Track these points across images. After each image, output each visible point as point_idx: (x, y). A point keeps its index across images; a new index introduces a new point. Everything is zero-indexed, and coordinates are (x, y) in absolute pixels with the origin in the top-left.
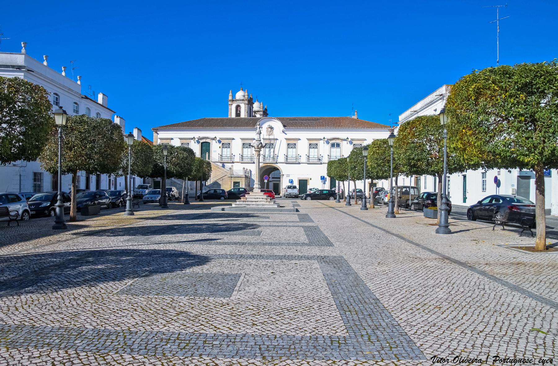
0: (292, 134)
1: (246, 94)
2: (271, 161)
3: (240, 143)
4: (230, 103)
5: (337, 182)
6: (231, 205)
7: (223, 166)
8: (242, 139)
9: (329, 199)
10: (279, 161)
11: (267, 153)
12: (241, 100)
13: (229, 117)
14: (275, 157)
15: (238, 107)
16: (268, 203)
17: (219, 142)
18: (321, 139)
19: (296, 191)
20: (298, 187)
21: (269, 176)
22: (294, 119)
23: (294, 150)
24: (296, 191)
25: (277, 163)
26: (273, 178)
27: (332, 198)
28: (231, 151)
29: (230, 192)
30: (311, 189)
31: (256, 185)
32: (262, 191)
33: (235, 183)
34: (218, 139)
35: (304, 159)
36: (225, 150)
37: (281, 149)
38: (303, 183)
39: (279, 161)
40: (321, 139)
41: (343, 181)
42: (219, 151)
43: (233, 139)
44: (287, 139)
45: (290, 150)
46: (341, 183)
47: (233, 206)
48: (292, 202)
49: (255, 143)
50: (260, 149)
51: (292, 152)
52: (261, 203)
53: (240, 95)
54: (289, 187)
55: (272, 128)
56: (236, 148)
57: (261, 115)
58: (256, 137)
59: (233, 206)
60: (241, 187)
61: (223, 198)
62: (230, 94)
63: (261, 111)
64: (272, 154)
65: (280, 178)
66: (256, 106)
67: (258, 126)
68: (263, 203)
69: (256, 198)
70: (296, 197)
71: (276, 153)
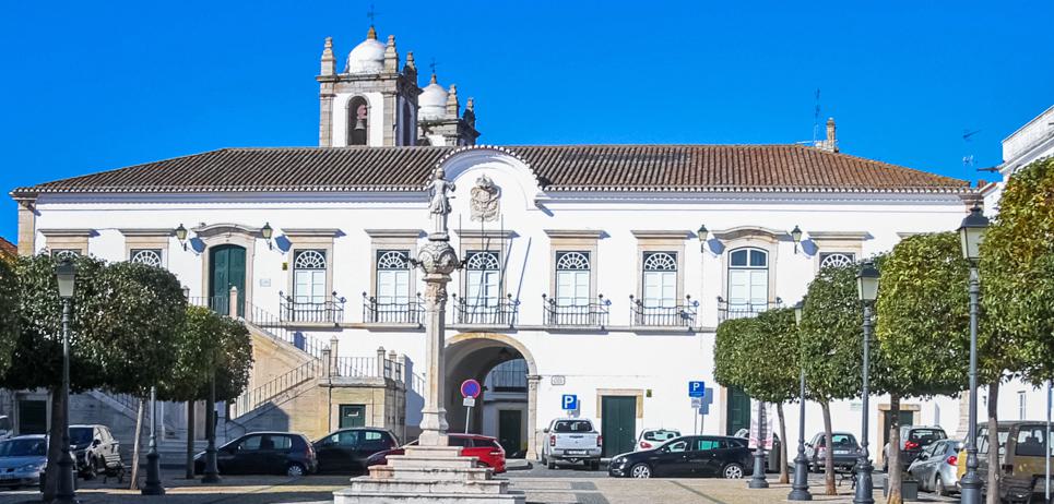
0: (575, 215)
1: (391, 53)
2: (490, 320)
4: (325, 89)
5: (755, 404)
7: (299, 343)
9: (721, 475)
11: (474, 291)
12: (369, 78)
13: (323, 144)
14: (507, 306)
16: (477, 490)
17: (284, 244)
18: (691, 235)
19: (589, 443)
20: (597, 425)
21: (480, 380)
22: (584, 155)
24: (589, 443)
25: (512, 329)
26: (497, 389)
27: (734, 470)
28: (329, 282)
29: (325, 447)
30: (649, 435)
31: (431, 418)
32: (452, 442)
33: (346, 409)
34: (277, 233)
35: (620, 314)
36: (305, 277)
37: (529, 276)
38: (619, 410)
39: (522, 320)
40: (691, 235)
41: (779, 401)
42: (282, 281)
43: (339, 234)
44: (553, 234)
45: (567, 278)
46: (771, 409)
48: (575, 486)
49: (424, 250)
50: (446, 272)
51: (573, 286)
52: (451, 489)
53: (364, 56)
54: (563, 427)
55: (492, 189)
56: (351, 268)
57: (448, 137)
58: (431, 225)
61: (296, 470)
62: (327, 53)
63: (448, 122)
64: (494, 292)
65: (524, 390)
66: (430, 102)
67: (439, 183)
68: (460, 489)
70: (591, 465)
71: (511, 288)
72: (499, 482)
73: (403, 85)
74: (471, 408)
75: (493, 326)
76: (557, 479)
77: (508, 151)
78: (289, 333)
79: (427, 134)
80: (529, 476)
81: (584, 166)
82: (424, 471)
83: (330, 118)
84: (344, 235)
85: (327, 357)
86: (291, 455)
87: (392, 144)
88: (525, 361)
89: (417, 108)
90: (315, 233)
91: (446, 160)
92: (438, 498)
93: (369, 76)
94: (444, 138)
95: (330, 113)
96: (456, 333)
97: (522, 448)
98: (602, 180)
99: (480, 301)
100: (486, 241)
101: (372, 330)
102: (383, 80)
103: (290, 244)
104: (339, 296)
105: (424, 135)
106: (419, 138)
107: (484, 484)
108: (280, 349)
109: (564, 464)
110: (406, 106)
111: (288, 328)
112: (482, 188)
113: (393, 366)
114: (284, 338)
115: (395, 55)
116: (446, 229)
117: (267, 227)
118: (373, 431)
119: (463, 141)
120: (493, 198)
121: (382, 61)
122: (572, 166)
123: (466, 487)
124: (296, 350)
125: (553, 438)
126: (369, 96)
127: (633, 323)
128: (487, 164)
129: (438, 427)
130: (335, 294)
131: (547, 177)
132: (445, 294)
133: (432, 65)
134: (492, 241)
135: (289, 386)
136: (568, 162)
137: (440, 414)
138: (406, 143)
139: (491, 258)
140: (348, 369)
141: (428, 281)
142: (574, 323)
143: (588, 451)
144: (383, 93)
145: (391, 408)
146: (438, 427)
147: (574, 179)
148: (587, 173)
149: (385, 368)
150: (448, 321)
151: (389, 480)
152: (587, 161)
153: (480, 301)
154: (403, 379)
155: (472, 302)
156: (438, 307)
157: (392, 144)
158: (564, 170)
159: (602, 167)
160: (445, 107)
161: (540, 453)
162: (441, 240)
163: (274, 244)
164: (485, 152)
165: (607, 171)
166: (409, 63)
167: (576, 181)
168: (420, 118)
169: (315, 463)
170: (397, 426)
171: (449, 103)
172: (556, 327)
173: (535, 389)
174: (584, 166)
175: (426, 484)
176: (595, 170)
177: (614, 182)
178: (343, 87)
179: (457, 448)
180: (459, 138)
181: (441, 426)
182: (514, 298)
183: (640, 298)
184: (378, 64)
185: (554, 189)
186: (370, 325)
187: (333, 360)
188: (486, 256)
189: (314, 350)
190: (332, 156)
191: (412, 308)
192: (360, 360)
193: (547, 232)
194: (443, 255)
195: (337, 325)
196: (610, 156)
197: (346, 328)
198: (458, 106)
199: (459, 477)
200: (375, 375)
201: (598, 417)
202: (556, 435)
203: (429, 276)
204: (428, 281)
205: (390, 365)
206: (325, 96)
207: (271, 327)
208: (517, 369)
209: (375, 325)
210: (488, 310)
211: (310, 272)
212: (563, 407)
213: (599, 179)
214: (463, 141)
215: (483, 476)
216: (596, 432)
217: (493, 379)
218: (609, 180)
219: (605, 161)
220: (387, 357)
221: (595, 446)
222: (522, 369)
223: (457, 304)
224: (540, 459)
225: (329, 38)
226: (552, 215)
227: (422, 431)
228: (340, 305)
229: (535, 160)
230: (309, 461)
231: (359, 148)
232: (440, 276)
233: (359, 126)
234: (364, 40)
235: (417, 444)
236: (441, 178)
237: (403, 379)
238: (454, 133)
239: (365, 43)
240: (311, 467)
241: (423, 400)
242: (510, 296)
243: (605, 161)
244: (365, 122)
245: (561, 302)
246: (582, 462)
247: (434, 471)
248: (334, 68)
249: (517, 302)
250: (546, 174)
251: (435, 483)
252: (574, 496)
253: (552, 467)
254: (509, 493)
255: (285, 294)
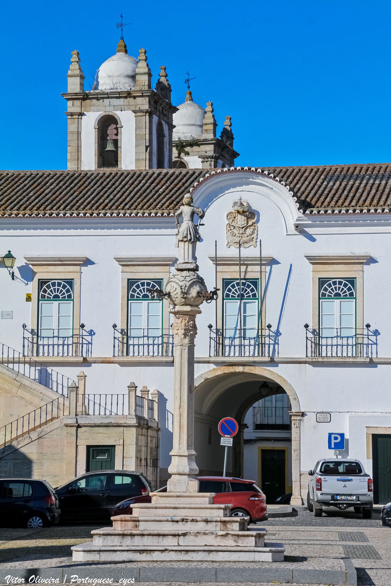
1: (142, 67)
2: (250, 353)
3: (119, 278)
4: (73, 107)
6: (66, 551)
7: (45, 380)
8: (125, 263)
10: (283, 353)
11: (231, 322)
13: (71, 167)
14: (267, 338)
15: (107, 124)
16: (230, 542)
17: (27, 273)
19: (359, 487)
20: (368, 467)
21: (240, 417)
23: (349, 305)
24: (359, 487)
25: (272, 362)
26: (259, 427)
28: (76, 314)
29: (69, 493)
31: (180, 461)
32: (204, 487)
33: (93, 451)
34: (20, 262)
36: (51, 308)
37: (291, 305)
39: (283, 353)
43: (87, 262)
44: (315, 261)
47: (78, 557)
48: (343, 537)
49: (175, 283)
50: (195, 304)
52: (201, 541)
53: (113, 72)
54: (329, 469)
55: (250, 214)
56: (101, 298)
57: (205, 158)
58: (181, 253)
59: (78, 557)
60: (118, 467)
62: (74, 68)
63: (205, 142)
64: (252, 323)
65: (287, 427)
66: (185, 122)
67: (186, 210)
68: (211, 540)
69: (182, 516)
70: (362, 512)
71: (271, 318)
72: (254, 533)
73: (156, 102)
74: (229, 447)
75: (251, 359)
76: (323, 528)
77: (266, 172)
78: (33, 369)
79: (182, 155)
80: (294, 524)
81: (348, 188)
82: (173, 521)
83: (79, 139)
84: (93, 263)
85: (73, 395)
86: (30, 504)
87: (144, 167)
88: (288, 396)
89: (172, 127)
90: (62, 262)
91: (200, 184)
92: (187, 551)
93: (119, 93)
94: (201, 160)
95: (79, 133)
96: (212, 366)
97: (287, 493)
98: (368, 202)
99: (238, 332)
100: (243, 268)
101: (123, 364)
102: (135, 97)
103: (34, 273)
104: (87, 328)
105: (179, 157)
106: (174, 159)
107: (238, 536)
108: (22, 386)
109: (334, 510)
110: (160, 125)
111: (31, 364)
112: (238, 212)
113: (146, 403)
114: (27, 374)
115: (146, 70)
116: (195, 258)
117: (9, 256)
118: (123, 474)
119: (220, 162)
120: (250, 223)
121: (133, 77)
122: (335, 187)
123: (219, 539)
124: (41, 388)
125: (319, 481)
126: (120, 115)
127: (212, 354)
128: (244, 187)
129: (187, 471)
130: (82, 326)
131: (308, 199)
132: (195, 327)
133: (187, 81)
134: (250, 268)
135: (32, 426)
136: (331, 184)
137: (189, 457)
138: (160, 165)
139: (249, 286)
140: (97, 406)
141: (175, 313)
142: (350, 354)
143: (358, 496)
144: (135, 112)
145: (143, 449)
146: (187, 471)
147: (337, 202)
148: (351, 194)
149: (136, 405)
150: (200, 353)
151: (134, 532)
152: (351, 182)
153: (238, 332)
154: (156, 417)
155: (229, 333)
156: (187, 341)
157: (144, 167)
158: (326, 192)
159: (368, 187)
160: (201, 126)
161: (305, 498)
162: (189, 270)
163: (17, 274)
164: (247, 175)
165: (374, 191)
166: (163, 79)
167: (340, 202)
168: (175, 137)
169: (57, 512)
170: (150, 469)
171: (205, 121)
172: (320, 360)
173: (299, 427)
174: (348, 188)
175: (174, 535)
176: (360, 190)
177: (381, 203)
178: (91, 106)
179: (208, 494)
180: (216, 159)
181: (191, 470)
182: (274, 329)
183: (125, 327)
184: (129, 80)
185: (315, 212)
186: (121, 359)
187: (80, 397)
188: (244, 284)
189: (60, 387)
190: (81, 179)
191: (165, 340)
192: (109, 397)
193: (309, 258)
194: (191, 286)
195: (85, 359)
196: (377, 176)
197: (95, 362)
198: (215, 125)
199: (211, 527)
200: (126, 413)
201: (368, 458)
202: (322, 478)
203: (178, 308)
204: (175, 313)
205: (142, 402)
206: (72, 114)
207: (13, 362)
208: (279, 404)
209: (126, 359)
210: (247, 342)
211: (56, 303)
212: (330, 447)
213: (365, 201)
214: (220, 162)
215: (236, 526)
216: (366, 475)
217: (254, 415)
218: (375, 201)
219: (371, 181)
220: (139, 394)
221: (365, 491)
222: (286, 405)
223: (214, 335)
224: (306, 505)
225: (75, 52)
226: (314, 240)
227: (170, 476)
228: (89, 338)
229: (295, 181)
230: (50, 510)
231: (108, 170)
232: (188, 308)
233: (110, 147)
234: (114, 54)
235: (165, 490)
236: (189, 204)
237: (156, 417)
238: (211, 153)
239: (113, 57)
240: (53, 517)
241: (172, 434)
242: (269, 326)
243: (371, 181)
244: (116, 143)
245: (325, 333)
246: (352, 509)
247: (183, 520)
248: (82, 85)
249: (278, 333)
250: (307, 196)
251: (184, 535)
252: (341, 550)
253: (319, 514)
254: (266, 545)
255: (29, 327)
